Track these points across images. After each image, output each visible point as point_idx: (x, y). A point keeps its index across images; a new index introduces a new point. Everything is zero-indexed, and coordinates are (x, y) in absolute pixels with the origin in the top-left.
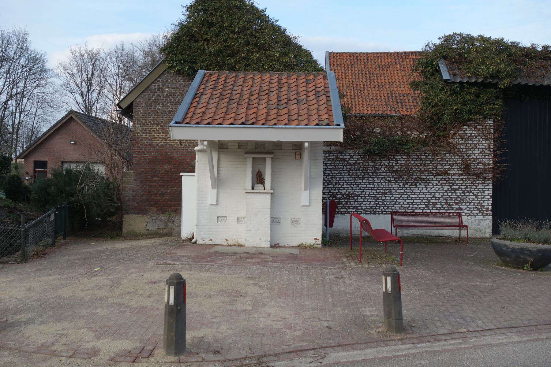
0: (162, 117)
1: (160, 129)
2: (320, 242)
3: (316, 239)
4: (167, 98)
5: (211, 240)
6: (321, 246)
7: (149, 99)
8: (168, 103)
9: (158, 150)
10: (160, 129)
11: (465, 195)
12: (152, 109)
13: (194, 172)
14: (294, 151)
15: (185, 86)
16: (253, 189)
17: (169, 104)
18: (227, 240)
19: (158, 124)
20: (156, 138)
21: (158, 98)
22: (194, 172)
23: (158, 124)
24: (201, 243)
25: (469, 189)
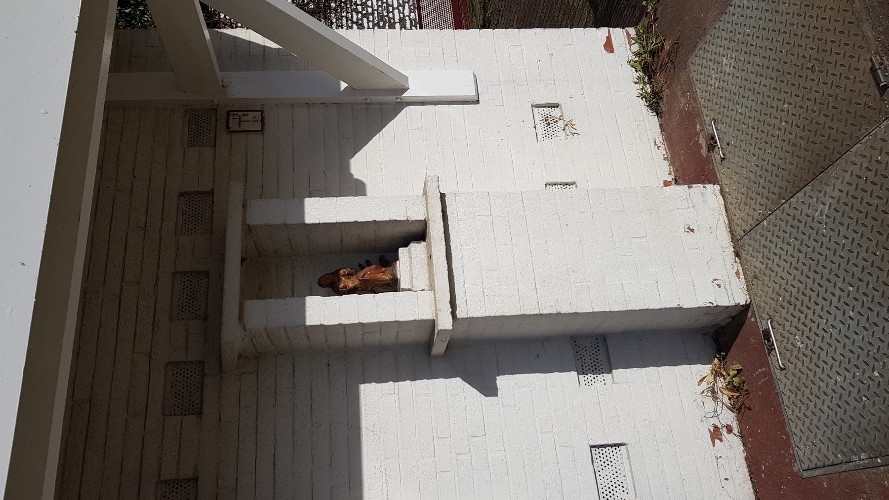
2: (618, 35)
3: (609, 46)
11: (372, 14)
18: (716, 434)
22: (496, 395)
25: (360, 8)
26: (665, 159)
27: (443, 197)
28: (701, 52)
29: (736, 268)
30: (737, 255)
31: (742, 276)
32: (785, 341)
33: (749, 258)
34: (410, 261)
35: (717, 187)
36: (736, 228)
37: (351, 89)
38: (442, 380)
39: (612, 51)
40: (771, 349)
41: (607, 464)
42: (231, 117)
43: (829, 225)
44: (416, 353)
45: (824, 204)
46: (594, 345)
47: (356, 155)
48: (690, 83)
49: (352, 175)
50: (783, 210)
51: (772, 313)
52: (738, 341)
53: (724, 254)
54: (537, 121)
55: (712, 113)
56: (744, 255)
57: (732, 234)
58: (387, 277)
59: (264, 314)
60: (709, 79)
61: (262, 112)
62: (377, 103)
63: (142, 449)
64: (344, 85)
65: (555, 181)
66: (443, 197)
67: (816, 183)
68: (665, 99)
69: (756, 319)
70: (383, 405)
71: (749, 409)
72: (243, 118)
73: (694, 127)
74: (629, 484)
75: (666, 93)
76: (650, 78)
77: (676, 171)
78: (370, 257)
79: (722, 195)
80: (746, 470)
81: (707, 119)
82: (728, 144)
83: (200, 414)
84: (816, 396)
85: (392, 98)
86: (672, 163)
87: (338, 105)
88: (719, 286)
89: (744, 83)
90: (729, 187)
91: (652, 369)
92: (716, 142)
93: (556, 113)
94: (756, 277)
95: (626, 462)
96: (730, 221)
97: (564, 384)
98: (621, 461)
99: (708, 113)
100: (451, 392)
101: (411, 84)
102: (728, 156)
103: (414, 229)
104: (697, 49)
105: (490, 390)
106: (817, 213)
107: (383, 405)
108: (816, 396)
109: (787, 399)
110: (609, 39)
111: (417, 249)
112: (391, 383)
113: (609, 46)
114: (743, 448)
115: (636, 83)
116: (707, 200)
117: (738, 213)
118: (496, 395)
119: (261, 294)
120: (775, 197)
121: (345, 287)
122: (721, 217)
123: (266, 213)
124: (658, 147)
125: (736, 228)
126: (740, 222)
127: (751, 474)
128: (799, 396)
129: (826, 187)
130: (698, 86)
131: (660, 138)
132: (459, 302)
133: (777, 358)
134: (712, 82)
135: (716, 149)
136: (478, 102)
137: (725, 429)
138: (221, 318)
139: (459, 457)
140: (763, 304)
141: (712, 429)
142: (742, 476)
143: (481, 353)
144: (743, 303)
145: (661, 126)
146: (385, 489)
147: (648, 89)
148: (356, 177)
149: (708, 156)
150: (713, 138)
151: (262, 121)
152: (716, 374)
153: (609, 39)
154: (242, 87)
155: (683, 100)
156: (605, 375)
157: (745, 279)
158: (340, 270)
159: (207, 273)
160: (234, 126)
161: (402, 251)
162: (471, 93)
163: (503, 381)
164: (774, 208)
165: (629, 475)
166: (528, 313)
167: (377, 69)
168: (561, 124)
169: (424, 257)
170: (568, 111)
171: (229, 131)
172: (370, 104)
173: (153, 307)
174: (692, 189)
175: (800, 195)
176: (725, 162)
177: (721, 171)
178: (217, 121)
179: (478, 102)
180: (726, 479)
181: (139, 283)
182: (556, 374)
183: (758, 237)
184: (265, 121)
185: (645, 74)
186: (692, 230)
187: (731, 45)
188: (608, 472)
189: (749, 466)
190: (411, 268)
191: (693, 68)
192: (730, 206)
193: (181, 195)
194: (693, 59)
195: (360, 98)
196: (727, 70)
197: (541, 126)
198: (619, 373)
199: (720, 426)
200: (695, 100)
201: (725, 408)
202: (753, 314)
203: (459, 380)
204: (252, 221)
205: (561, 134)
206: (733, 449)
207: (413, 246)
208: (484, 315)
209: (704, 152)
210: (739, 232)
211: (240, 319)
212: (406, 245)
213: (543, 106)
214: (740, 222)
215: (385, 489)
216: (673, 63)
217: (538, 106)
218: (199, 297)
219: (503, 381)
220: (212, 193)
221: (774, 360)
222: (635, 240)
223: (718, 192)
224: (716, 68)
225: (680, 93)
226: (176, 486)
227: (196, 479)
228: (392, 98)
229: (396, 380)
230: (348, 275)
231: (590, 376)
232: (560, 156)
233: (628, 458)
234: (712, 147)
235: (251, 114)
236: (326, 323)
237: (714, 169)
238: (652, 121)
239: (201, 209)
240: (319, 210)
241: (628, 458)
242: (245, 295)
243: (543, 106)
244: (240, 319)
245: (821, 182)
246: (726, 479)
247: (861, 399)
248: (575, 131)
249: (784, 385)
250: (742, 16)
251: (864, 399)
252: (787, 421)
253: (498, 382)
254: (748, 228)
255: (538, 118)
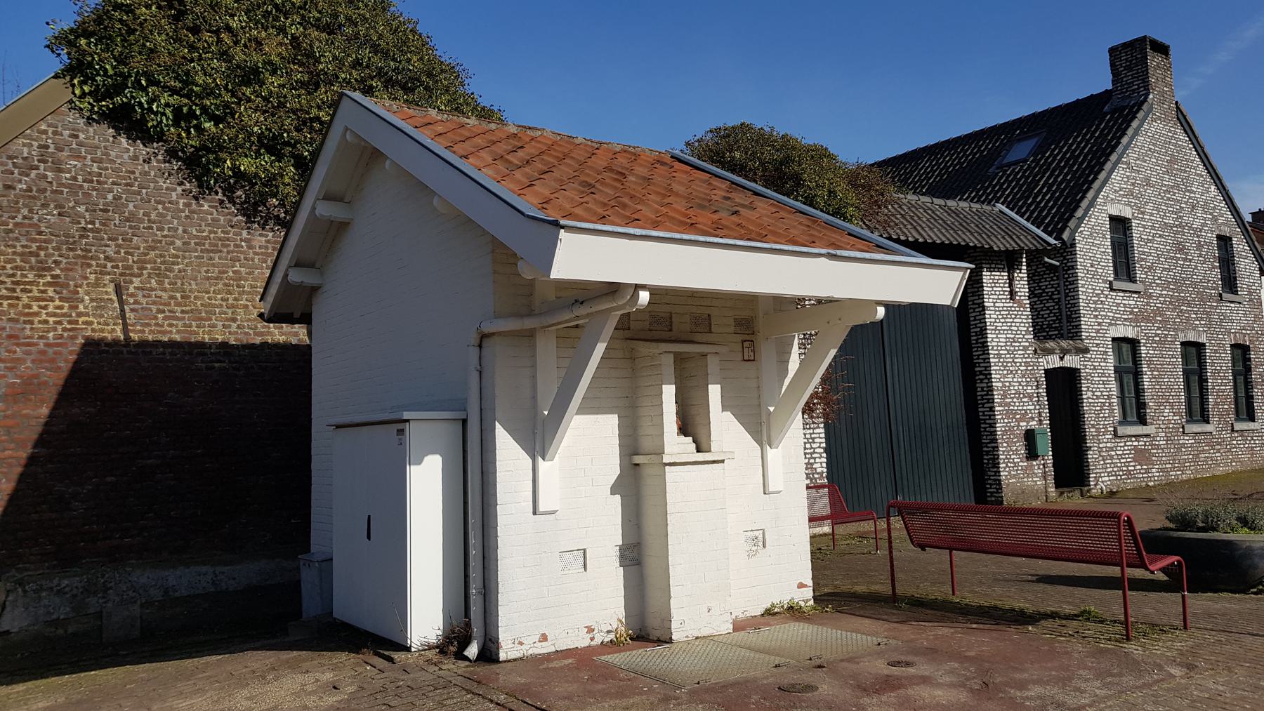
0: (58, 249)
1: (49, 284)
2: (809, 593)
3: (801, 586)
4: (74, 189)
5: (544, 638)
6: (811, 603)
7: (8, 187)
8: (77, 203)
9: (43, 352)
10: (49, 284)
12: (19, 220)
13: (1047, 371)
14: (739, 338)
15: (135, 158)
17: (81, 209)
18: (590, 630)
19: (42, 269)
20: (36, 314)
21: (43, 185)
23: (42, 269)
24: (512, 655)
27: (723, 461)
37: (769, 413)
39: (1219, 237)
46: (640, 556)
59: (669, 361)
62: (760, 428)
64: (772, 409)
66: (723, 461)
85: (765, 438)
97: (615, 536)
100: (612, 467)
103: (704, 446)
110: (806, 586)
113: (801, 586)
123: (713, 364)
131: (748, 614)
148: (426, 459)
153: (806, 586)
154: (767, 351)
160: (746, 344)
163: (618, 497)
167: (783, 429)
171: (743, 341)
195: (764, 419)
198: (499, 580)
219: (618, 497)
228: (765, 438)
240: (715, 391)
255: (757, 533)
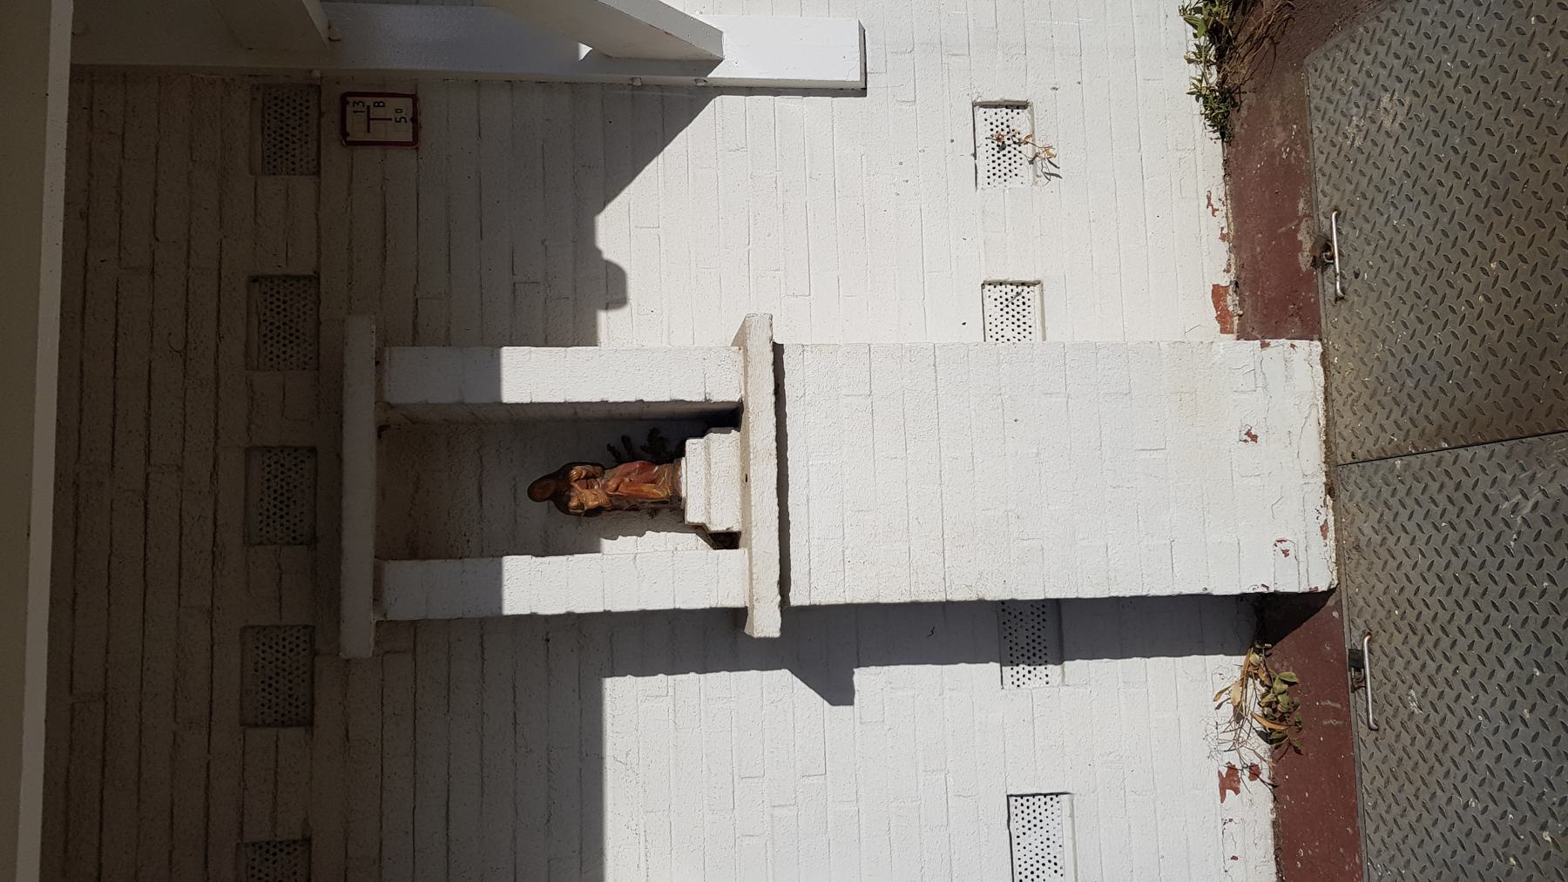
16: (726, 540)
18: (1229, 781)
22: (851, 703)
26: (1223, 237)
27: (778, 350)
28: (1339, 55)
29: (1322, 518)
30: (1330, 491)
31: (1331, 534)
32: (1389, 686)
33: (1351, 506)
34: (708, 474)
35: (1317, 347)
36: (1340, 441)
38: (754, 673)
40: (1360, 684)
41: (1031, 825)
42: (349, 109)
43: (1524, 539)
44: (704, 640)
45: (1526, 497)
47: (610, 207)
48: (1299, 109)
49: (599, 252)
50: (1441, 459)
51: (1375, 627)
52: (1300, 632)
53: (1306, 488)
54: (981, 139)
55: (1337, 196)
56: (1344, 496)
57: (1328, 448)
58: (661, 493)
59: (421, 589)
60: (1344, 121)
61: (415, 98)
63: (207, 788)
64: (585, 50)
65: (1002, 278)
66: (778, 350)
67: (1520, 448)
68: (1244, 112)
69: (1341, 615)
70: (634, 707)
71: (1298, 751)
72: (377, 112)
73: (1294, 199)
74: (1066, 859)
75: (1248, 99)
76: (1220, 55)
77: (1240, 267)
78: (632, 458)
79: (1323, 364)
80: (1270, 842)
81: (1324, 203)
82: (1357, 275)
83: (309, 723)
84: (1424, 805)
86: (1236, 248)
87: (573, 85)
88: (1286, 553)
89: (1415, 171)
90: (1341, 358)
91: (1136, 662)
92: (1332, 258)
93: (1020, 121)
94: (1357, 548)
95: (1067, 823)
96: (1330, 423)
97: (974, 683)
98: (1058, 820)
99: (1328, 189)
101: (729, 49)
102: (1352, 297)
104: (1331, 43)
105: (839, 692)
106: (1506, 505)
107: (634, 707)
108: (1424, 805)
109: (1369, 780)
111: (721, 443)
112: (661, 676)
114: (1271, 805)
115: (1190, 61)
116: (1296, 366)
117: (1348, 417)
118: (851, 703)
119: (414, 550)
120: (1430, 429)
121: (581, 506)
122: (1314, 411)
123: (422, 380)
124: (1214, 211)
125: (1340, 441)
126: (1347, 433)
127: (1278, 849)
128: (1394, 787)
129: (1536, 467)
130: (1317, 122)
131: (1219, 192)
132: (795, 575)
133: (1365, 705)
134: (1350, 130)
135: (1330, 271)
136: (862, 92)
137: (1246, 772)
138: (338, 609)
139: (777, 811)
140: (1361, 603)
141: (1224, 771)
142: (1262, 853)
143: (830, 645)
144: (1323, 587)
145: (1226, 162)
146: (643, 865)
147: (1214, 78)
148: (607, 255)
149: (1309, 273)
150: (1328, 247)
151: (414, 120)
152: (1248, 674)
155: (1281, 136)
156: (1050, 667)
157: (1337, 540)
158: (570, 466)
159: (313, 450)
160: (357, 131)
161: (692, 445)
162: (854, 76)
163: (866, 679)
164: (1422, 446)
165: (1068, 844)
166: (924, 598)
168: (1028, 150)
169: (734, 462)
170: (1046, 125)
172: (643, 87)
173: (211, 517)
174: (1268, 350)
175: (1482, 452)
176: (1343, 306)
177: (1330, 317)
178: (321, 115)
179: (862, 92)
180: (1234, 858)
181: (180, 468)
182: (962, 667)
183: (1378, 481)
184: (422, 119)
185: (1212, 41)
186: (1254, 438)
187: (1406, 75)
188: (1033, 838)
189: (1276, 836)
190: (708, 484)
191: (1313, 78)
192: (1335, 394)
193: (255, 280)
194: (1315, 58)
196: (1387, 124)
197: (986, 149)
199: (1238, 766)
200: (1306, 147)
201: (1254, 734)
202: (1338, 606)
203: (785, 673)
204: (393, 397)
205: (1026, 171)
206: (1256, 806)
207: (715, 438)
208: (841, 601)
209: (1304, 260)
210: (1343, 454)
211: (377, 599)
212: (701, 434)
213: (996, 105)
214: (1347, 433)
215: (643, 865)
216: (1274, 44)
217: (986, 105)
218: (294, 500)
219: (866, 679)
220: (315, 278)
221: (1361, 704)
222: (1144, 455)
223: (1317, 359)
224: (1359, 101)
225: (1277, 116)
226: (272, 850)
227: (308, 841)
229: (671, 671)
230: (586, 477)
231: (1023, 669)
232: (1018, 224)
233: (1072, 816)
234: (1322, 260)
235: (392, 103)
236: (542, 611)
237: (1317, 302)
238: (1212, 150)
239: (293, 319)
240: (532, 376)
241: (1072, 816)
242: (385, 553)
243: (996, 105)
244: (377, 599)
245: (1529, 452)
246: (1234, 858)
247: (1507, 860)
248: (1053, 170)
249: (1370, 755)
250: (1444, 25)
251: (1512, 861)
252: (1361, 811)
253: (855, 678)
254: (1361, 454)
255: (984, 131)
